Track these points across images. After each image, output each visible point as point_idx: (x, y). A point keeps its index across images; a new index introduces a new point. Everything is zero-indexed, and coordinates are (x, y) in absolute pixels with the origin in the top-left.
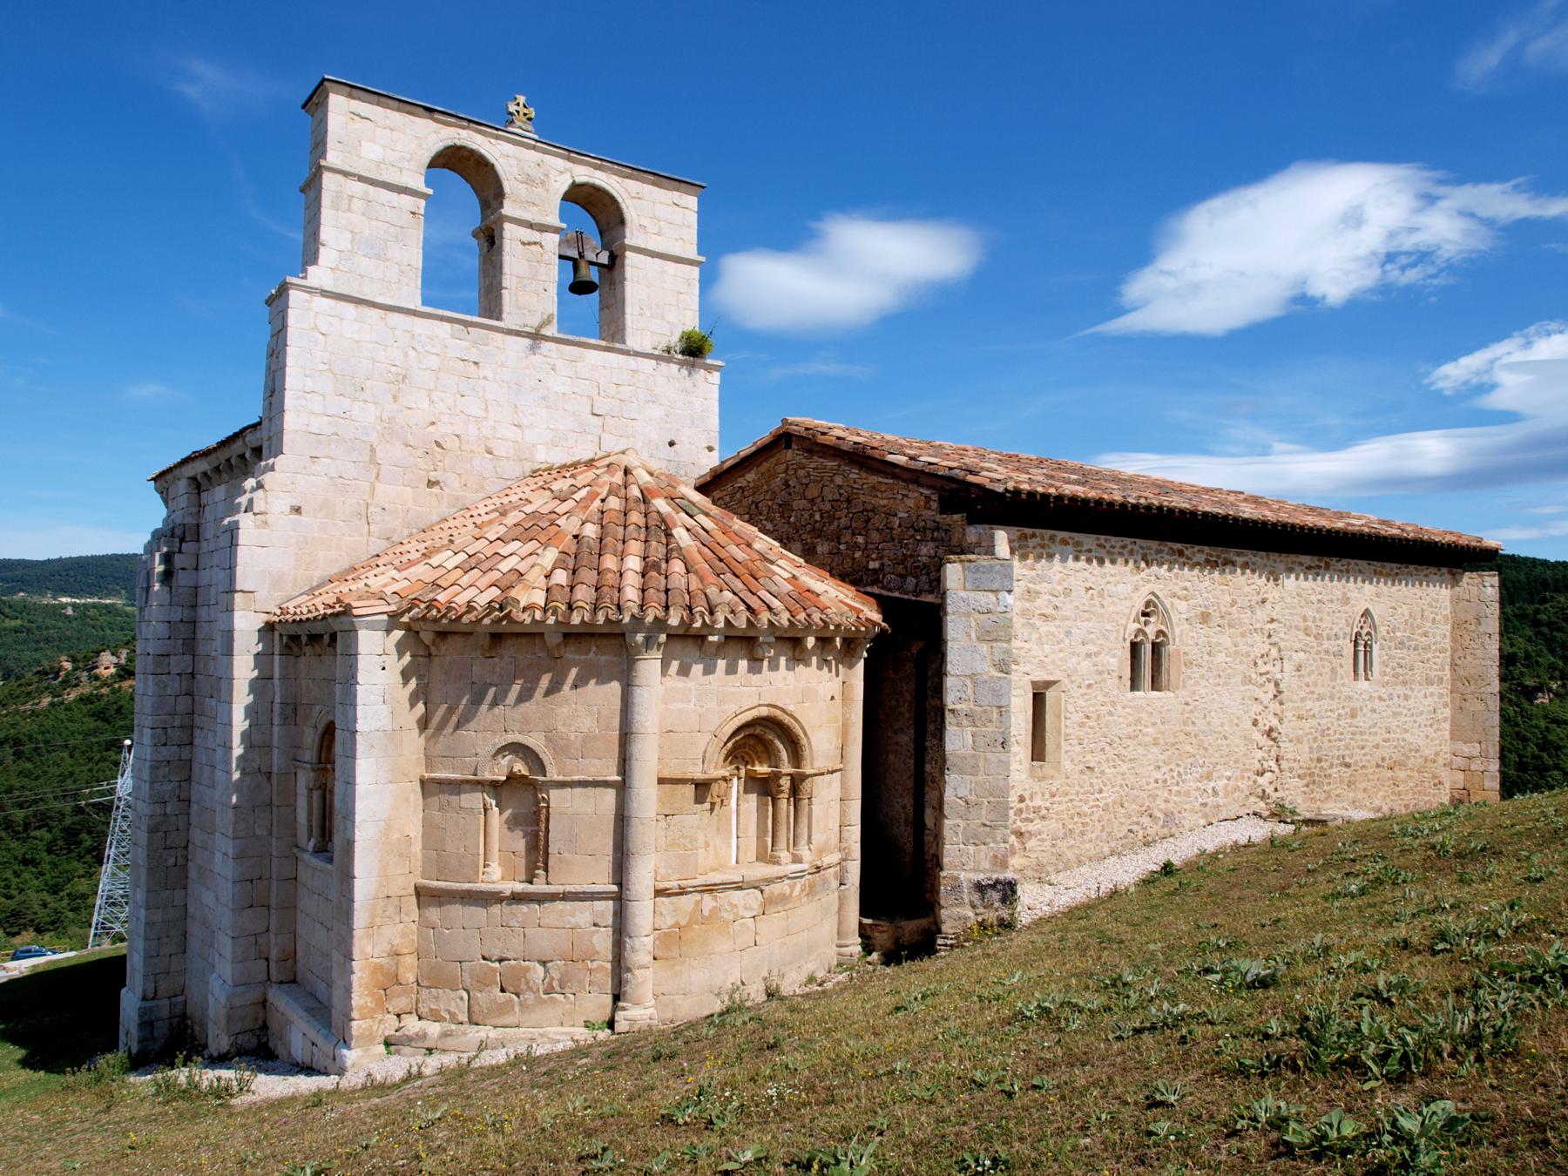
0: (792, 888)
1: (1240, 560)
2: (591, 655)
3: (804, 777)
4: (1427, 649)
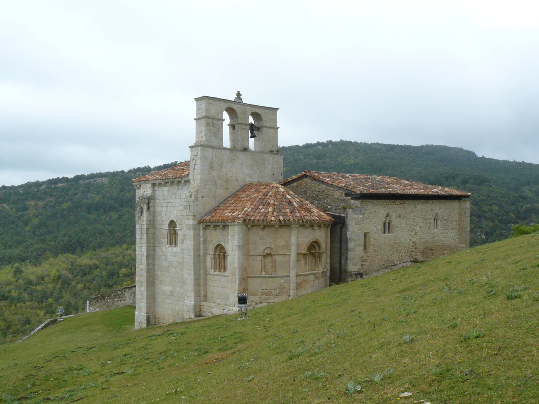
1: (407, 203)
3: (321, 253)
4: (452, 221)
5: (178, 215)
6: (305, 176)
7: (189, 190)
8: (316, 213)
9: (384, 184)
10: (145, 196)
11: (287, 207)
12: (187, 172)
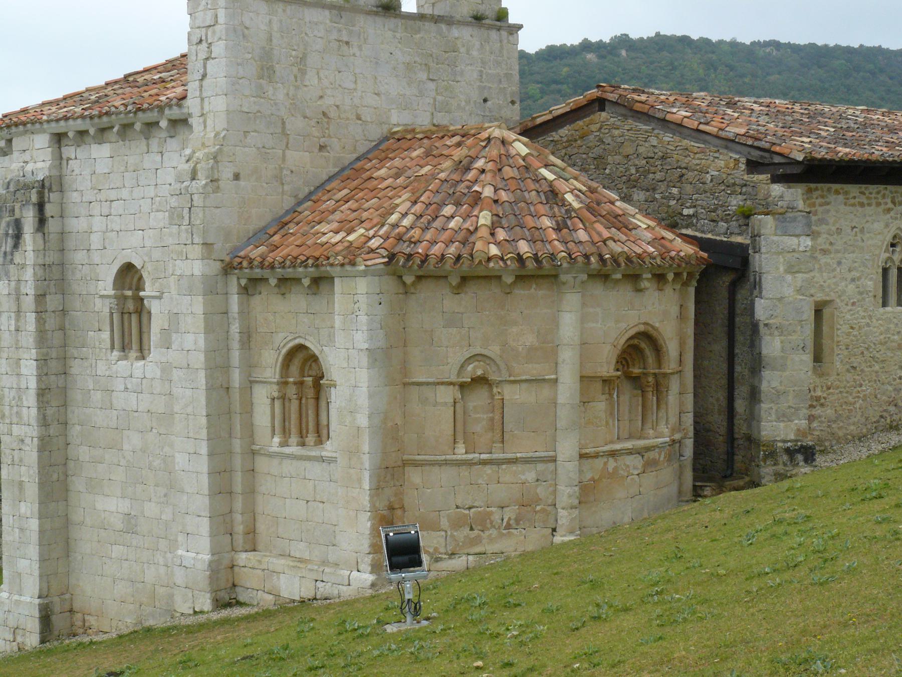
0: (660, 454)
2: (533, 290)
3: (665, 375)
5: (148, 243)
6: (600, 103)
7: (188, 152)
8: (644, 234)
9: (878, 132)
10: (29, 178)
11: (542, 209)
12: (179, 90)
